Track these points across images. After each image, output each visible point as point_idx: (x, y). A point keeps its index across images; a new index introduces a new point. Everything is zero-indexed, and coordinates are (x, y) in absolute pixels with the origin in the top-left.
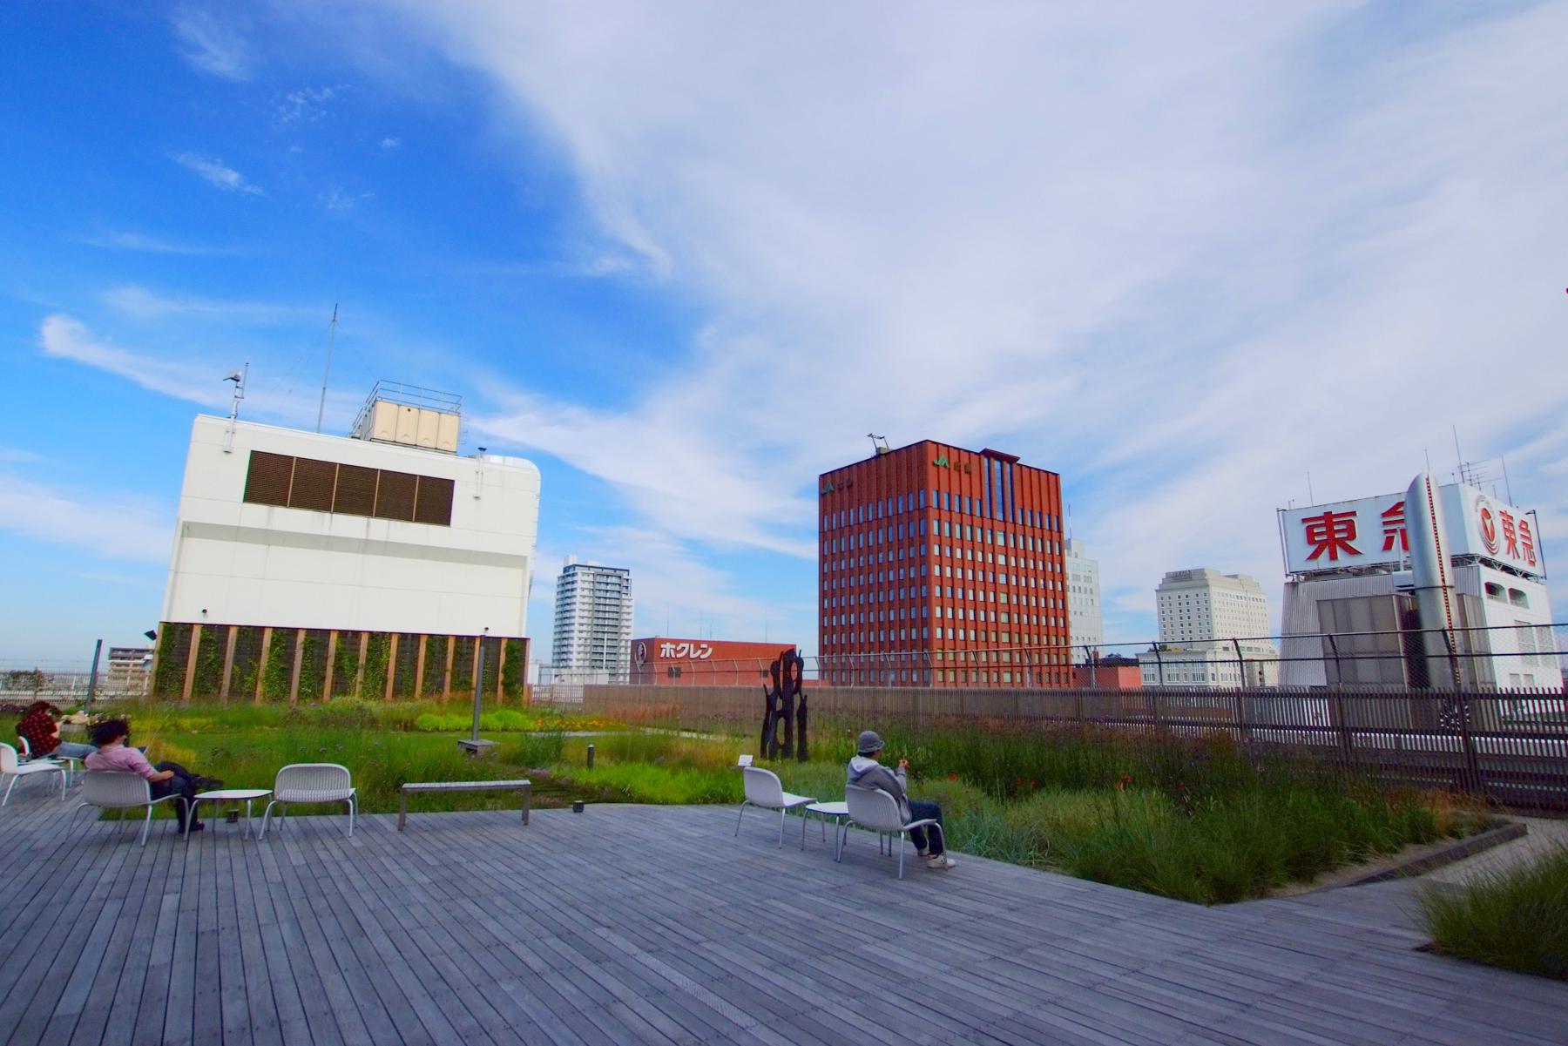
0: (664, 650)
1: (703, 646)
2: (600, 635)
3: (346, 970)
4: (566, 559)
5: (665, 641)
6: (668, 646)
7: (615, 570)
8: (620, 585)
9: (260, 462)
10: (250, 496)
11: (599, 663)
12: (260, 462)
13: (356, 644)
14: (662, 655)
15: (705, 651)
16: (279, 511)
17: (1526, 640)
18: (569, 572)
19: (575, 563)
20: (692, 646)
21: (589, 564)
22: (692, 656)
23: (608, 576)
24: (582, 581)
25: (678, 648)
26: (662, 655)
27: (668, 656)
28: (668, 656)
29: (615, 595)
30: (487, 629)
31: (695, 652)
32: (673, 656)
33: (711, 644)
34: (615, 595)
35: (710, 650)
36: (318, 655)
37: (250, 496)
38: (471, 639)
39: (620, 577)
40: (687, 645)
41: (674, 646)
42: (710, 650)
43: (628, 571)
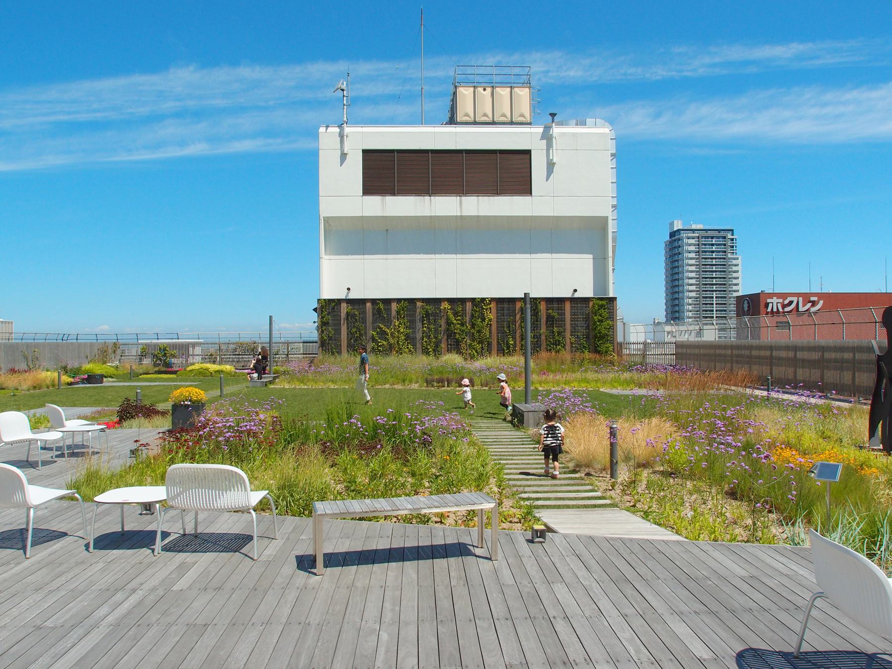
0: (770, 305)
1: (812, 299)
2: (708, 294)
3: (408, 537)
4: (672, 224)
5: (771, 295)
6: (775, 300)
7: (719, 231)
8: (725, 245)
9: (523, 186)
10: (368, 190)
11: (708, 314)
12: (523, 186)
13: (678, 312)
14: (769, 309)
15: (814, 304)
16: (390, 199)
17: (496, 387)
18: (675, 240)
19: (680, 227)
20: (801, 299)
21: (694, 227)
22: (801, 309)
23: (712, 238)
24: (689, 246)
25: (786, 302)
26: (769, 309)
27: (775, 310)
28: (775, 310)
29: (721, 255)
30: (575, 291)
31: (804, 305)
32: (781, 309)
33: (821, 296)
34: (721, 255)
35: (821, 302)
36: (434, 316)
37: (368, 190)
38: (561, 301)
39: (725, 238)
40: (795, 299)
41: (781, 300)
42: (821, 302)
43: (732, 230)
